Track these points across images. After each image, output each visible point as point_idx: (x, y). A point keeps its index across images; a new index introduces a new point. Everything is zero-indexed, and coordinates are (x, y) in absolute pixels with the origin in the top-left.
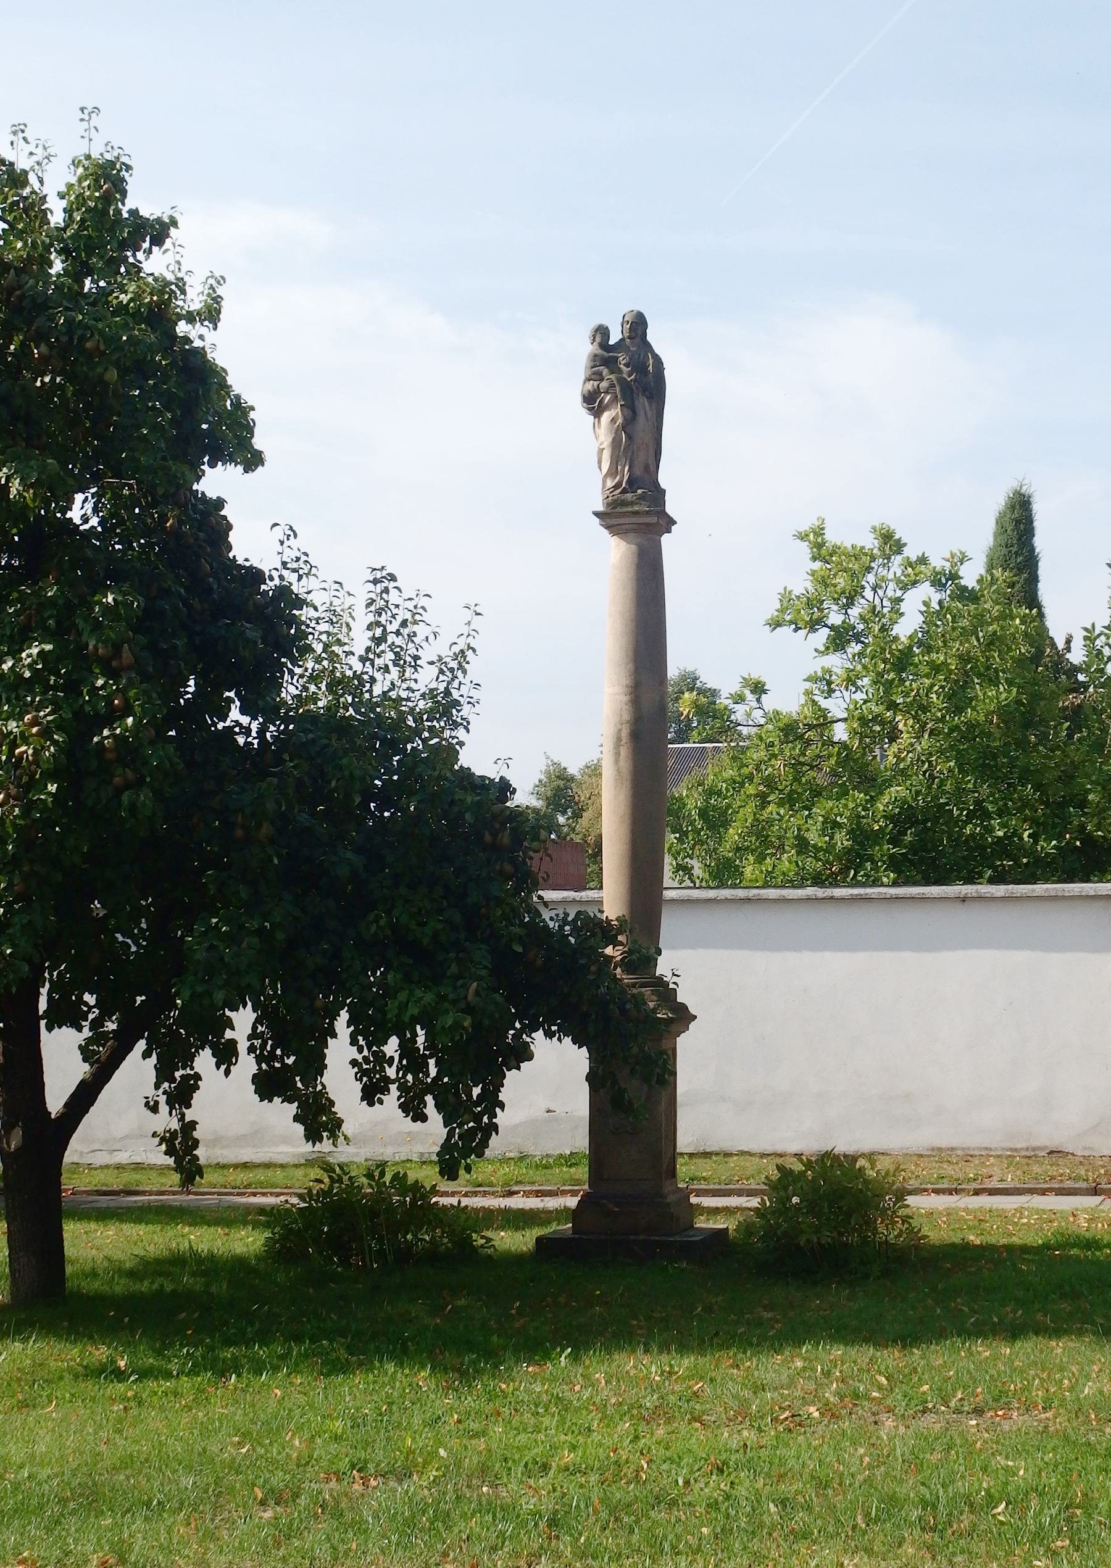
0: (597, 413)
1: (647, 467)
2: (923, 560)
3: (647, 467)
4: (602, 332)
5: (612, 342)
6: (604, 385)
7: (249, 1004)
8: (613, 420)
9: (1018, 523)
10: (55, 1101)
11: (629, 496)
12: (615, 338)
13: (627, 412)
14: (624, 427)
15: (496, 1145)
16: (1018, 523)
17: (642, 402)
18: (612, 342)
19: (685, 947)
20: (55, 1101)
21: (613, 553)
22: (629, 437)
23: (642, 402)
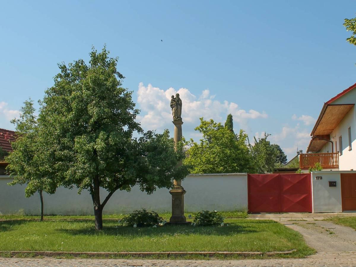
0: (172, 108)
1: (179, 115)
2: (216, 124)
3: (179, 115)
4: (173, 97)
5: (174, 98)
6: (174, 104)
7: (157, 187)
8: (175, 109)
9: (230, 118)
10: (101, 203)
11: (177, 119)
12: (175, 97)
13: (177, 108)
14: (176, 110)
15: (324, 219)
16: (230, 118)
17: (179, 106)
18: (174, 98)
19: (345, 148)
20: (101, 203)
21: (49, 214)
22: (177, 111)
23: (179, 106)
